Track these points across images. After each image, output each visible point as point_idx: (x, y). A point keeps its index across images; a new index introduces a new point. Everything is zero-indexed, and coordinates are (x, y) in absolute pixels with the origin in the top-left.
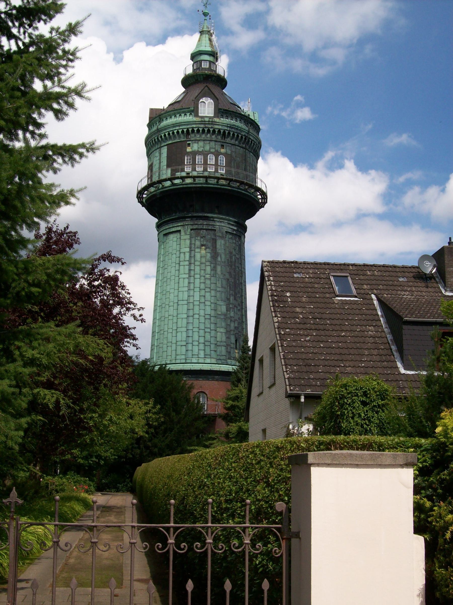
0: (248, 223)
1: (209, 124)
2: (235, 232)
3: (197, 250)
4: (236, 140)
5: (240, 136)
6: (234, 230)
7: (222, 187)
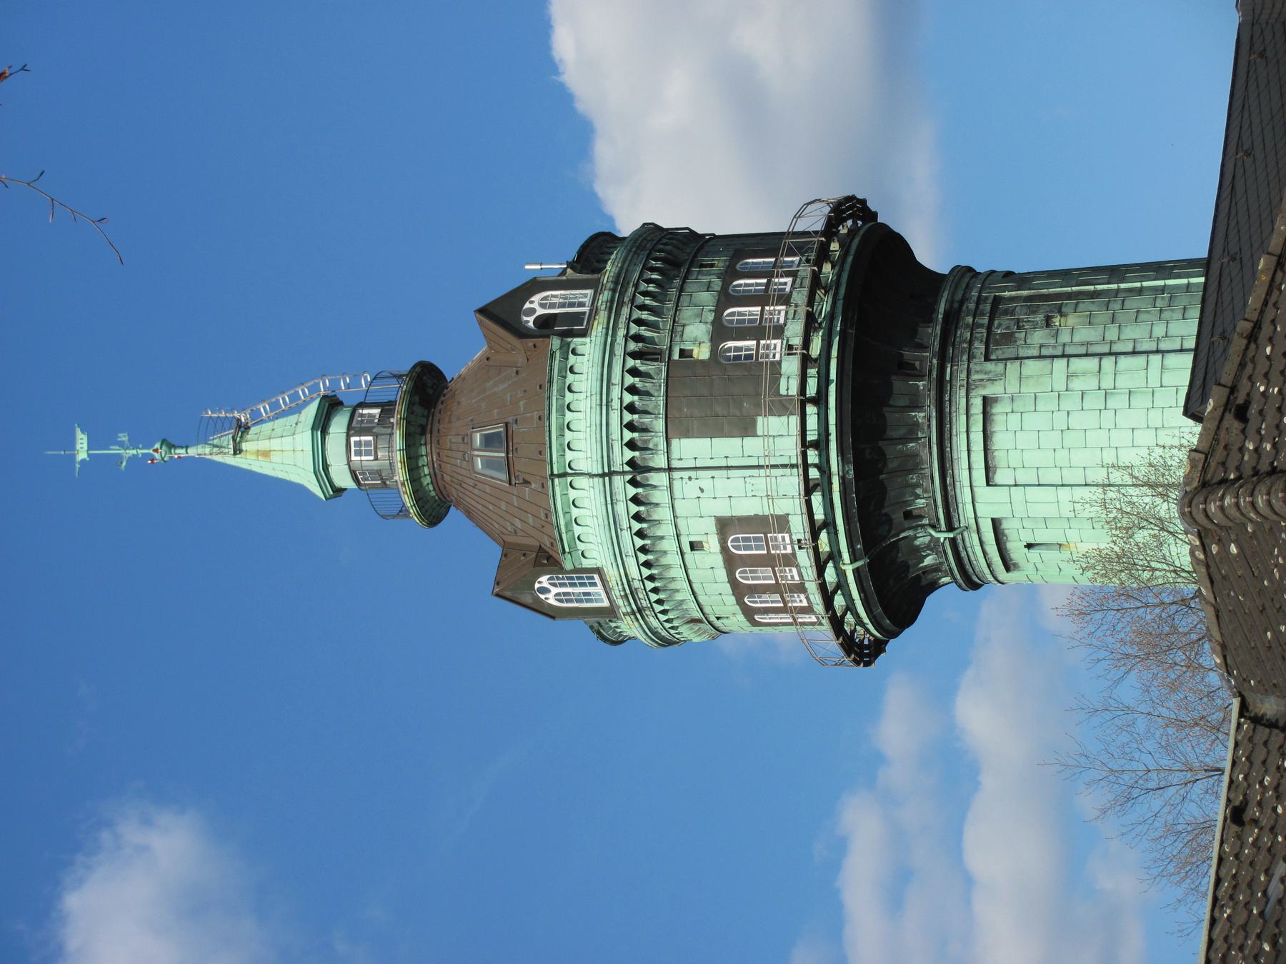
1: (622, 294)
3: (1065, 337)
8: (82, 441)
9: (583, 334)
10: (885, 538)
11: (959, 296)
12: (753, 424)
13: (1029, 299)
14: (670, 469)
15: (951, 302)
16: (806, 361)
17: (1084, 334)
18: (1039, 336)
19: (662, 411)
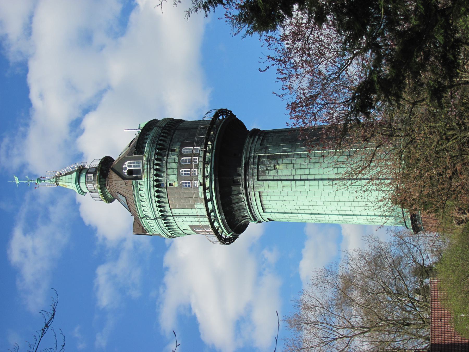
0: (249, 128)
1: (150, 165)
2: (261, 137)
3: (280, 173)
4: (161, 176)
5: (162, 134)
6: (259, 138)
7: (214, 148)
8: (16, 179)
9: (141, 179)
10: (238, 223)
11: (248, 156)
12: (194, 205)
13: (268, 157)
14: (173, 216)
15: (246, 159)
16: (205, 189)
17: (286, 172)
18: (272, 172)
19: (167, 201)
